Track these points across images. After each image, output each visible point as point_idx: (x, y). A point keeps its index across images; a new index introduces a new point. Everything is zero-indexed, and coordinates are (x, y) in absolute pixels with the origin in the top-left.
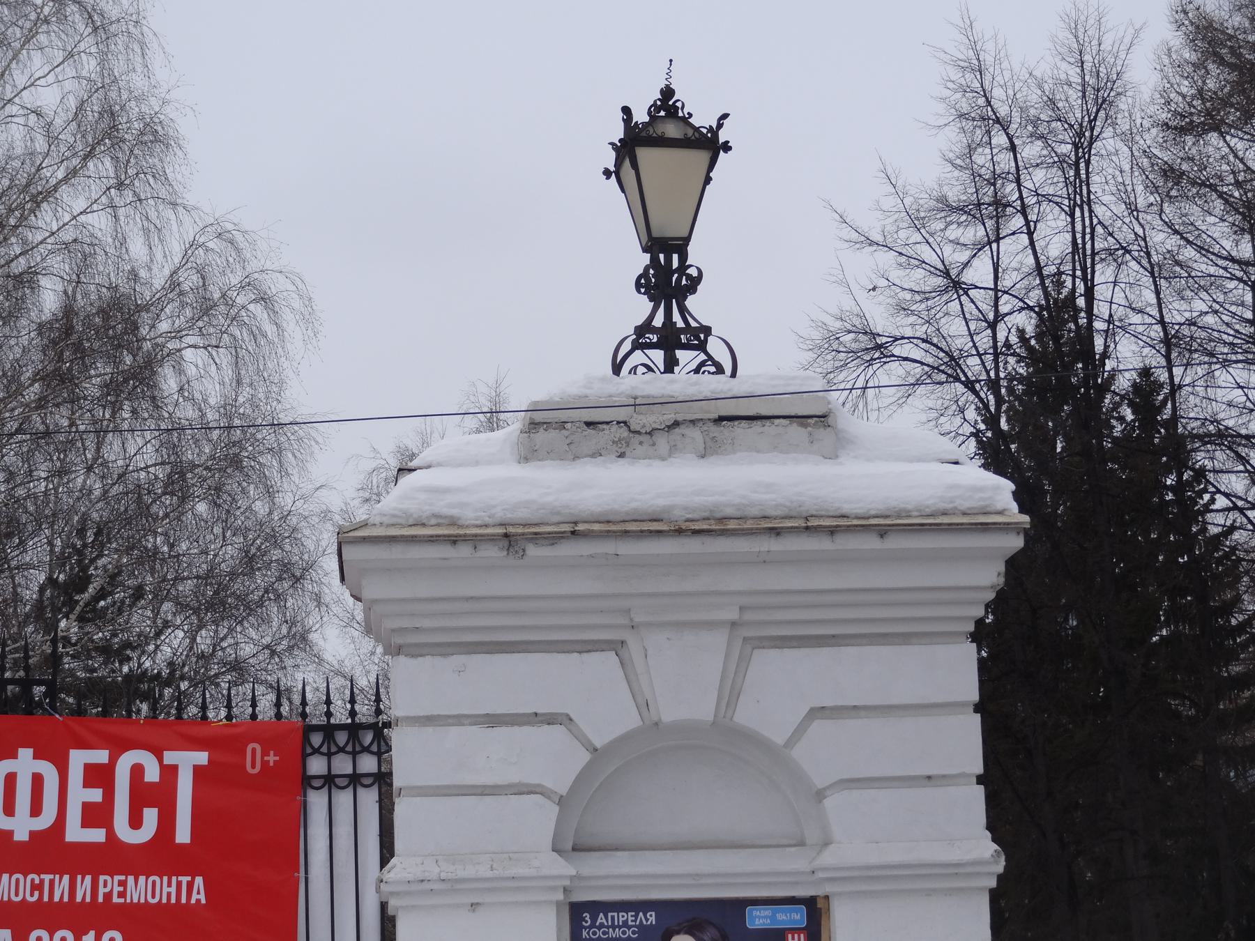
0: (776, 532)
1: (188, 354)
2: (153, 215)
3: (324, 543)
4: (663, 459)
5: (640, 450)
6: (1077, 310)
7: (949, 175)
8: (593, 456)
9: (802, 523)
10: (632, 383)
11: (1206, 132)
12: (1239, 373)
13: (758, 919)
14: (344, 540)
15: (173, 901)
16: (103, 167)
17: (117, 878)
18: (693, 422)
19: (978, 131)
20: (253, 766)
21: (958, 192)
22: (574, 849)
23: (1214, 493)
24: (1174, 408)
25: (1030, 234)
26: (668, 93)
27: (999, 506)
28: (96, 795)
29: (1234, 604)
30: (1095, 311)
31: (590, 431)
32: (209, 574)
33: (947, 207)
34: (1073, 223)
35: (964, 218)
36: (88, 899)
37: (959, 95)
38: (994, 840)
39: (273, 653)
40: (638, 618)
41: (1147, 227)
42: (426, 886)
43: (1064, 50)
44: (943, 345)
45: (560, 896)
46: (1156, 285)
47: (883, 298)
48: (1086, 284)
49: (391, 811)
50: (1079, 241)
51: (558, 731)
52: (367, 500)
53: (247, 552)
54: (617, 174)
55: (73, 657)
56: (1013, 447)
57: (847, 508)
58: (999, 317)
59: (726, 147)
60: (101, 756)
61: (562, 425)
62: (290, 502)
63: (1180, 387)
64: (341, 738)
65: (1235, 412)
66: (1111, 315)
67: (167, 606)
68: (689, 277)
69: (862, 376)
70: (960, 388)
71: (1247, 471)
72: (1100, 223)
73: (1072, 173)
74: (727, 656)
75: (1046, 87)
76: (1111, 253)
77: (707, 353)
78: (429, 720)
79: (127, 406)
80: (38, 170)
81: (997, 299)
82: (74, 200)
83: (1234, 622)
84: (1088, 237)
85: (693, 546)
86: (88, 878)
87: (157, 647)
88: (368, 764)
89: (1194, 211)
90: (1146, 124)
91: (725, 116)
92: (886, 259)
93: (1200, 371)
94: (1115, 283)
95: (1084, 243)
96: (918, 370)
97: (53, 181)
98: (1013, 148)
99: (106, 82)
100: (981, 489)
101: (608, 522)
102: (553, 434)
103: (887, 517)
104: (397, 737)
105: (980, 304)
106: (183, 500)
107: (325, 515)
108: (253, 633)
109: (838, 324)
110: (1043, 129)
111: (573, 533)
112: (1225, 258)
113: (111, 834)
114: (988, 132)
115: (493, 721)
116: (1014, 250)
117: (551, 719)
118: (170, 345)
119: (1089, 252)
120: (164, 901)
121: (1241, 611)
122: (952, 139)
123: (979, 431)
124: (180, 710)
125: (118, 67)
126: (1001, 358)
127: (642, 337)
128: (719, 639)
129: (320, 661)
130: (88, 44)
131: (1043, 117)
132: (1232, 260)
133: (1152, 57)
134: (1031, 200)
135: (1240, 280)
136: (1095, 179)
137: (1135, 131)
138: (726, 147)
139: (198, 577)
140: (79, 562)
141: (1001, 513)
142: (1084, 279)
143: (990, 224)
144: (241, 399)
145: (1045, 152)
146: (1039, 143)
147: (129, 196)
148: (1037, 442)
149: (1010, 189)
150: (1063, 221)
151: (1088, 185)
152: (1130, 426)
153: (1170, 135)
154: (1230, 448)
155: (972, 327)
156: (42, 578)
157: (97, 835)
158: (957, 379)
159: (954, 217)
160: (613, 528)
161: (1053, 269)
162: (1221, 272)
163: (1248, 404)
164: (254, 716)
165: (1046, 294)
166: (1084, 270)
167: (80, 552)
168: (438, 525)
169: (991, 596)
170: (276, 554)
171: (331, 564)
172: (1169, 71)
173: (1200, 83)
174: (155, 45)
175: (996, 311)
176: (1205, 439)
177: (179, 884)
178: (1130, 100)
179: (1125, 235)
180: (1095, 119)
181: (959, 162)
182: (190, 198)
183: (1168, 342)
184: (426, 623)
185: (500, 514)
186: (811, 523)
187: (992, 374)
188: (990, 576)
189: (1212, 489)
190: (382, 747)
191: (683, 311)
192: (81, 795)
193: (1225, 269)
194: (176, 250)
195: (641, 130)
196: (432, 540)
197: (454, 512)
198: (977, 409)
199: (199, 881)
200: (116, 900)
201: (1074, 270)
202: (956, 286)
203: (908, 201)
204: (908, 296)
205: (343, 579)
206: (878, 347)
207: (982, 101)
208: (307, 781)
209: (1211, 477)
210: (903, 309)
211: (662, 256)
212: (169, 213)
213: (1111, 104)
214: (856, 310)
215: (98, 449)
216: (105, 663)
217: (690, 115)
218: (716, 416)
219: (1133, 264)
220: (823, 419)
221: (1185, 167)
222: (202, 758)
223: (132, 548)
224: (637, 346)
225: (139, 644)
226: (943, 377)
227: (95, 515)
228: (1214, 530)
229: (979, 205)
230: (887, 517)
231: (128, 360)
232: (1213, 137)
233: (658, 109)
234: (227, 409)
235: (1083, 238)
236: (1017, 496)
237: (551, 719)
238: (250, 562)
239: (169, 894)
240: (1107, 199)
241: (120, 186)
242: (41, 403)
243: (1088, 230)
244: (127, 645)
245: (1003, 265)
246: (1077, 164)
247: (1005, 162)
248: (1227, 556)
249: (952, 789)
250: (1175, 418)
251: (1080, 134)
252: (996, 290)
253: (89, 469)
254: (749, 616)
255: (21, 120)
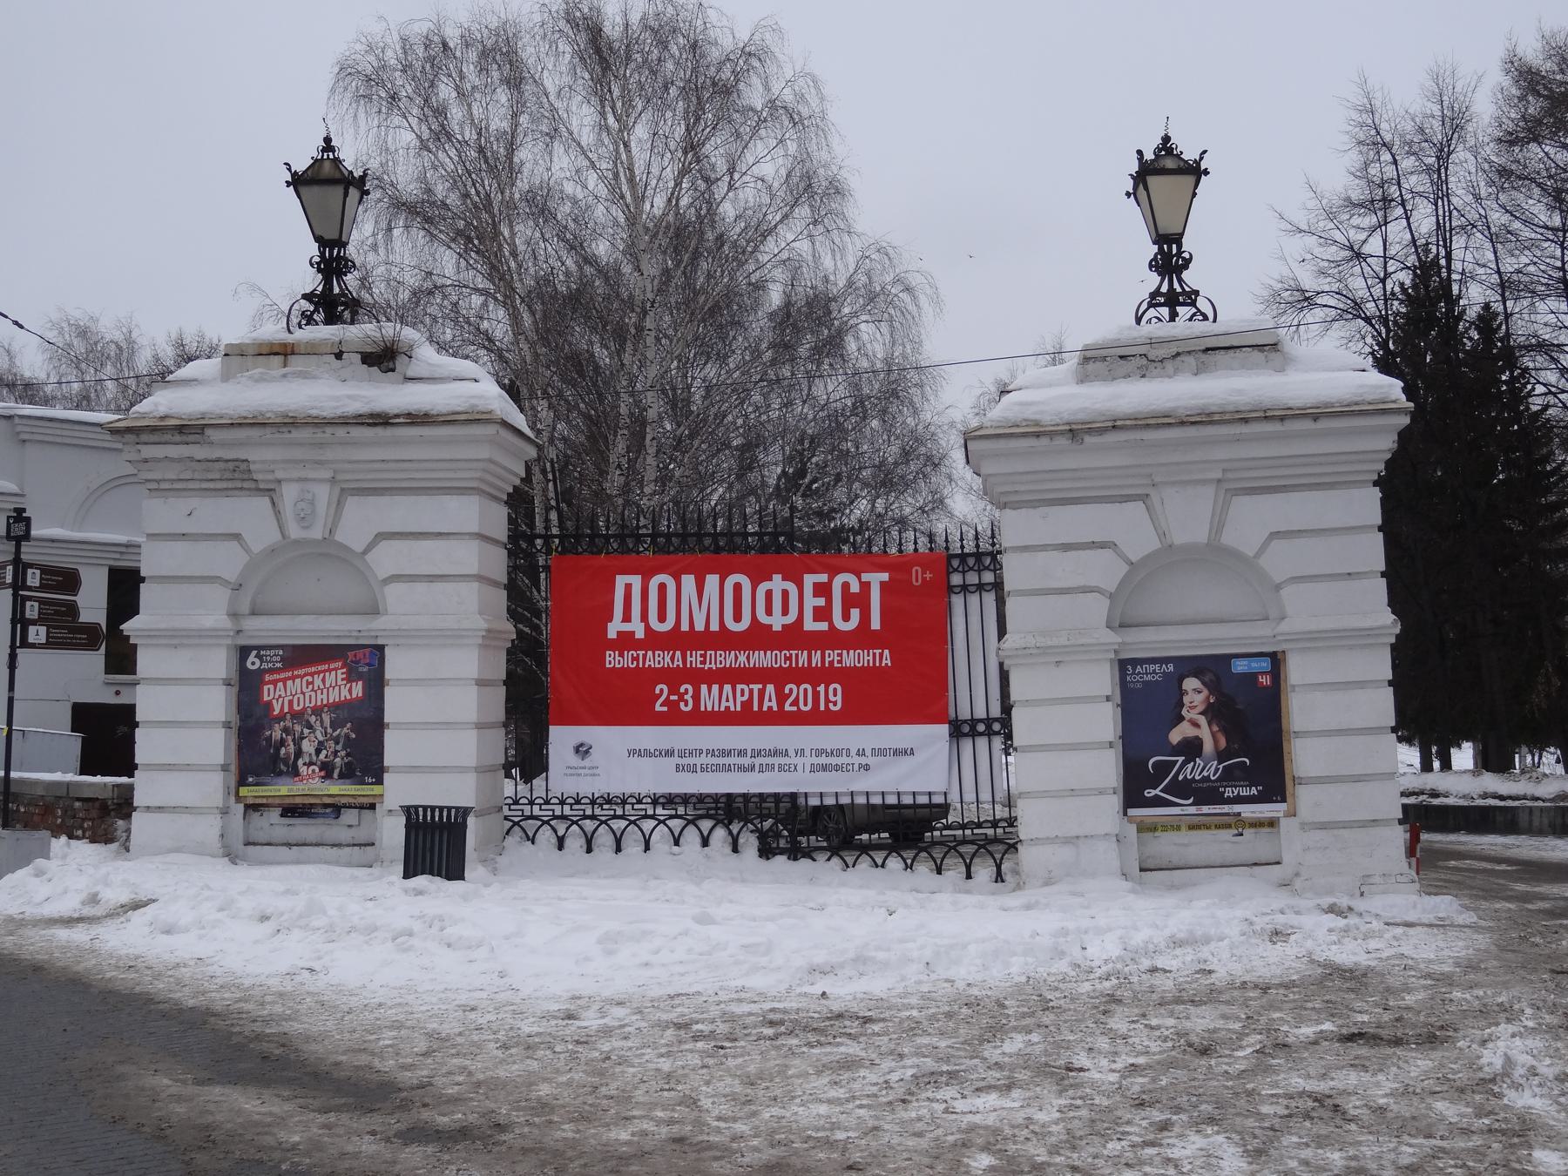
0: (1245, 421)
1: (863, 326)
2: (837, 240)
3: (952, 442)
4: (1170, 377)
5: (1155, 372)
6: (1440, 268)
7: (1352, 183)
8: (1124, 377)
9: (1262, 414)
10: (1149, 329)
11: (1528, 143)
12: (1553, 303)
13: (1240, 667)
14: (968, 438)
15: (871, 665)
16: (803, 211)
17: (836, 652)
18: (1189, 352)
19: (1371, 152)
20: (917, 581)
21: (1358, 192)
22: (1121, 626)
23: (1535, 384)
24: (1507, 328)
25: (1408, 219)
26: (1166, 139)
27: (1393, 398)
28: (821, 602)
29: (1547, 458)
30: (1453, 268)
31: (1122, 362)
32: (882, 463)
33: (1351, 204)
34: (1437, 210)
35: (1363, 210)
36: (819, 665)
37: (1358, 129)
38: (1393, 613)
39: (924, 512)
40: (1157, 479)
41: (1488, 209)
42: (1028, 651)
43: (1429, 94)
44: (1350, 295)
45: (229, 641)
46: (1494, 248)
47: (1309, 266)
48: (1446, 250)
49: (1004, 603)
50: (1441, 221)
51: (1107, 553)
52: (977, 414)
53: (904, 449)
54: (1135, 194)
55: (800, 518)
56: (1398, 360)
57: (1291, 403)
58: (1387, 275)
59: (1206, 172)
60: (823, 578)
61: (1104, 359)
62: (929, 417)
63: (1511, 314)
64: (971, 561)
65: (1549, 329)
66: (1463, 270)
67: (857, 485)
68: (1184, 259)
69: (1296, 318)
70: (1362, 323)
71: (1558, 368)
72: (1455, 208)
73: (1436, 176)
74: (1215, 502)
75: (1417, 120)
76: (1463, 227)
77: (1196, 308)
78: (1026, 549)
79: (827, 361)
80: (764, 216)
81: (1386, 263)
82: (787, 234)
83: (1548, 468)
84: (1447, 218)
85: (1192, 432)
86: (819, 652)
87: (851, 511)
88: (988, 577)
89: (1520, 197)
90: (1487, 140)
91: (1205, 152)
92: (1311, 241)
93: (1525, 303)
94: (1466, 248)
95: (1444, 223)
96: (1333, 313)
97: (773, 223)
98: (1395, 162)
99: (803, 158)
100: (1381, 387)
101: (1136, 419)
102: (1099, 365)
103: (1318, 408)
104: (1005, 560)
105: (1374, 267)
106: (864, 418)
107: (952, 424)
108: (910, 500)
109: (1280, 285)
110: (1415, 148)
111: (1114, 427)
112: (1542, 227)
113: (831, 625)
114: (1378, 152)
115: (1067, 547)
116: (1396, 230)
117: (1103, 545)
118: (851, 322)
119: (1448, 229)
120: (866, 665)
121: (1554, 461)
122: (1354, 159)
123: (1374, 350)
124: (870, 546)
125: (813, 147)
126: (1389, 302)
127: (1154, 299)
128: (1210, 491)
129: (951, 515)
130: (790, 134)
131: (1415, 140)
132: (1547, 227)
133: (1490, 94)
134: (1407, 196)
135: (1552, 241)
136: (1451, 179)
137: (1478, 145)
138: (1206, 172)
139: (874, 466)
140: (801, 461)
141: (1394, 402)
142: (1445, 246)
143: (1380, 214)
144: (896, 354)
145: (1417, 164)
146: (1413, 158)
147: (820, 228)
148: (1414, 358)
149: (1393, 191)
150: (1430, 208)
151: (1447, 184)
152: (1476, 344)
153: (1504, 147)
154: (1546, 353)
155: (1369, 283)
156: (779, 470)
157: (823, 626)
158: (1359, 317)
159: (1356, 210)
160: (1140, 423)
161: (1424, 241)
162: (1539, 236)
163: (1559, 323)
164: (916, 550)
165: (1419, 259)
166: (1445, 240)
167: (801, 454)
168: (1027, 426)
169: (1389, 456)
170: (923, 450)
171: (958, 456)
172: (1501, 102)
173: (1523, 110)
174: (833, 130)
175: (1386, 270)
176: (1529, 348)
177: (874, 654)
178: (1475, 125)
179: (1473, 216)
180: (1451, 139)
181: (1358, 174)
182: (858, 228)
183: (1502, 285)
184: (1022, 488)
185: (1066, 417)
186: (1269, 414)
187: (1383, 313)
188: (1386, 444)
189: (1533, 381)
190: (996, 567)
191: (1180, 281)
192: (811, 602)
193: (1542, 234)
194: (851, 261)
195: (1150, 165)
196: (1024, 435)
197: (1038, 417)
198: (1373, 336)
199: (886, 652)
200: (836, 665)
201: (1438, 241)
202: (1358, 256)
203: (1324, 202)
204: (1326, 264)
205: (968, 462)
206: (1307, 299)
207: (1373, 132)
208: (950, 589)
209: (1533, 373)
210: (1322, 273)
211: (1165, 246)
212: (846, 238)
213: (1462, 128)
214: (1291, 275)
215: (810, 389)
216: (820, 522)
217: (1182, 153)
218: (1203, 348)
219: (1478, 234)
220: (1274, 346)
221: (1514, 167)
222: (885, 576)
223: (833, 450)
224: (1151, 305)
225: (840, 508)
226: (1351, 316)
227: (810, 432)
228: (1534, 408)
229: (1373, 201)
230: (1318, 408)
231: (826, 332)
232: (1533, 146)
233: (1160, 150)
234: (888, 361)
235: (1444, 219)
236: (1404, 390)
237: (1103, 545)
238: (906, 455)
239: (691, 656)
240: (1459, 192)
241: (815, 223)
242: (773, 362)
243: (1447, 214)
244: (833, 510)
245: (1390, 240)
246: (1439, 170)
247: (1390, 172)
248: (1544, 425)
249: (1365, 582)
250: (1508, 334)
251: (1441, 150)
252: (1385, 257)
253: (804, 402)
254: (1230, 475)
255: (752, 185)
